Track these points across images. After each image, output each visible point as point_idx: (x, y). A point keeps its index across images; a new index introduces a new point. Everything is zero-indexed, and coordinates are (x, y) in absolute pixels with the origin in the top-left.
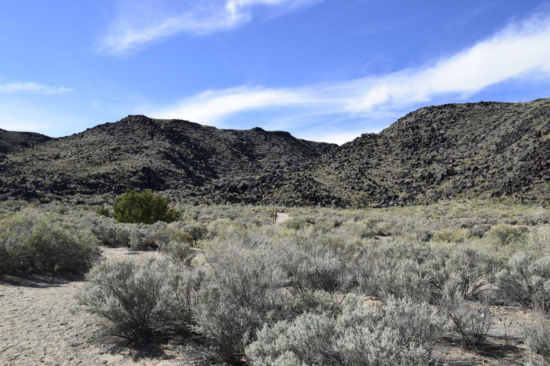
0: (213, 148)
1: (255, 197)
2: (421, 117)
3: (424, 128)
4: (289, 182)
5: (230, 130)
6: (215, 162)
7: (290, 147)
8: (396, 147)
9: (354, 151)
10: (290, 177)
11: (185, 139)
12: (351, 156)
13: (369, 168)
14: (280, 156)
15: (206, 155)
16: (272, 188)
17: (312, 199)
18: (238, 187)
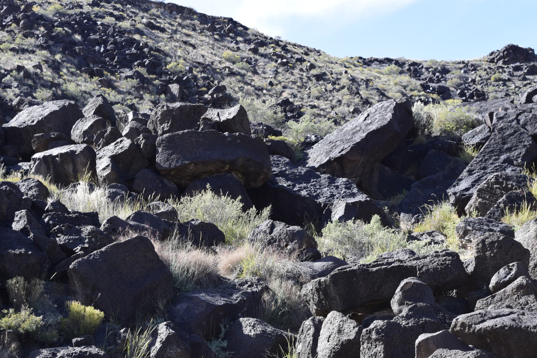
11: (141, 56)
18: (317, 157)
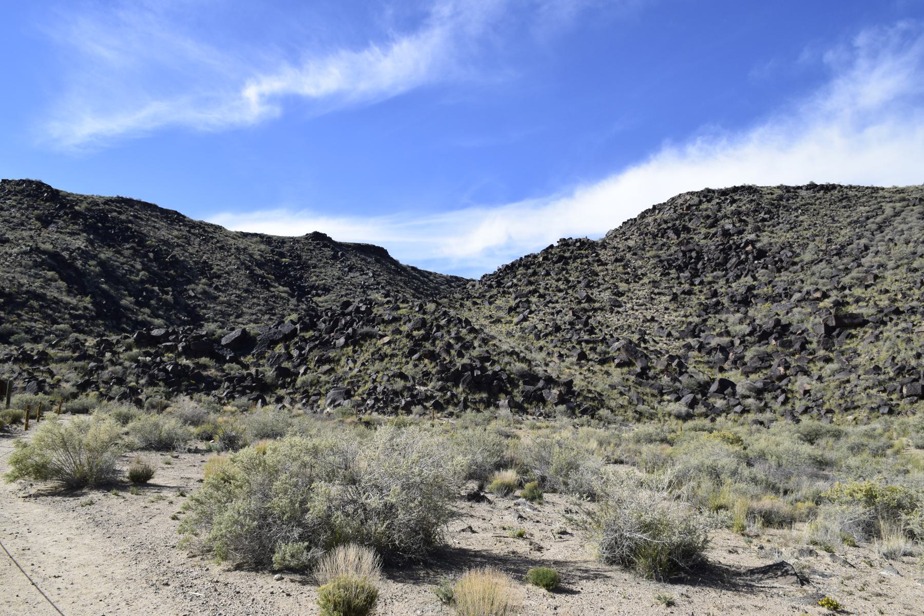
0: (205, 262)
1: (270, 373)
2: (689, 208)
3: (703, 231)
4: (391, 328)
5: (256, 235)
6: (204, 293)
7: (386, 277)
8: (646, 264)
9: (548, 274)
10: (395, 314)
11: (133, 237)
12: (543, 284)
13: (595, 310)
14: (364, 292)
15: (182, 276)
16: (334, 347)
17: (476, 385)
18: (224, 342)
